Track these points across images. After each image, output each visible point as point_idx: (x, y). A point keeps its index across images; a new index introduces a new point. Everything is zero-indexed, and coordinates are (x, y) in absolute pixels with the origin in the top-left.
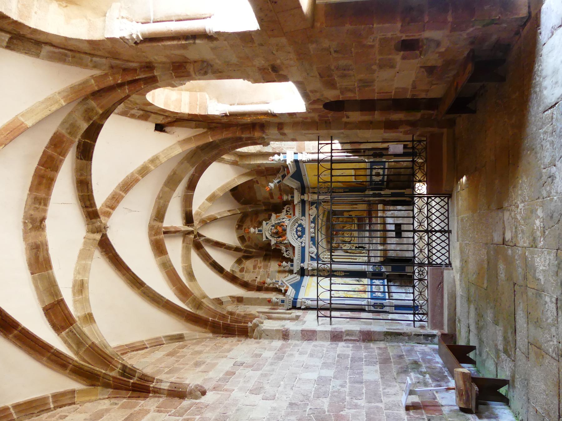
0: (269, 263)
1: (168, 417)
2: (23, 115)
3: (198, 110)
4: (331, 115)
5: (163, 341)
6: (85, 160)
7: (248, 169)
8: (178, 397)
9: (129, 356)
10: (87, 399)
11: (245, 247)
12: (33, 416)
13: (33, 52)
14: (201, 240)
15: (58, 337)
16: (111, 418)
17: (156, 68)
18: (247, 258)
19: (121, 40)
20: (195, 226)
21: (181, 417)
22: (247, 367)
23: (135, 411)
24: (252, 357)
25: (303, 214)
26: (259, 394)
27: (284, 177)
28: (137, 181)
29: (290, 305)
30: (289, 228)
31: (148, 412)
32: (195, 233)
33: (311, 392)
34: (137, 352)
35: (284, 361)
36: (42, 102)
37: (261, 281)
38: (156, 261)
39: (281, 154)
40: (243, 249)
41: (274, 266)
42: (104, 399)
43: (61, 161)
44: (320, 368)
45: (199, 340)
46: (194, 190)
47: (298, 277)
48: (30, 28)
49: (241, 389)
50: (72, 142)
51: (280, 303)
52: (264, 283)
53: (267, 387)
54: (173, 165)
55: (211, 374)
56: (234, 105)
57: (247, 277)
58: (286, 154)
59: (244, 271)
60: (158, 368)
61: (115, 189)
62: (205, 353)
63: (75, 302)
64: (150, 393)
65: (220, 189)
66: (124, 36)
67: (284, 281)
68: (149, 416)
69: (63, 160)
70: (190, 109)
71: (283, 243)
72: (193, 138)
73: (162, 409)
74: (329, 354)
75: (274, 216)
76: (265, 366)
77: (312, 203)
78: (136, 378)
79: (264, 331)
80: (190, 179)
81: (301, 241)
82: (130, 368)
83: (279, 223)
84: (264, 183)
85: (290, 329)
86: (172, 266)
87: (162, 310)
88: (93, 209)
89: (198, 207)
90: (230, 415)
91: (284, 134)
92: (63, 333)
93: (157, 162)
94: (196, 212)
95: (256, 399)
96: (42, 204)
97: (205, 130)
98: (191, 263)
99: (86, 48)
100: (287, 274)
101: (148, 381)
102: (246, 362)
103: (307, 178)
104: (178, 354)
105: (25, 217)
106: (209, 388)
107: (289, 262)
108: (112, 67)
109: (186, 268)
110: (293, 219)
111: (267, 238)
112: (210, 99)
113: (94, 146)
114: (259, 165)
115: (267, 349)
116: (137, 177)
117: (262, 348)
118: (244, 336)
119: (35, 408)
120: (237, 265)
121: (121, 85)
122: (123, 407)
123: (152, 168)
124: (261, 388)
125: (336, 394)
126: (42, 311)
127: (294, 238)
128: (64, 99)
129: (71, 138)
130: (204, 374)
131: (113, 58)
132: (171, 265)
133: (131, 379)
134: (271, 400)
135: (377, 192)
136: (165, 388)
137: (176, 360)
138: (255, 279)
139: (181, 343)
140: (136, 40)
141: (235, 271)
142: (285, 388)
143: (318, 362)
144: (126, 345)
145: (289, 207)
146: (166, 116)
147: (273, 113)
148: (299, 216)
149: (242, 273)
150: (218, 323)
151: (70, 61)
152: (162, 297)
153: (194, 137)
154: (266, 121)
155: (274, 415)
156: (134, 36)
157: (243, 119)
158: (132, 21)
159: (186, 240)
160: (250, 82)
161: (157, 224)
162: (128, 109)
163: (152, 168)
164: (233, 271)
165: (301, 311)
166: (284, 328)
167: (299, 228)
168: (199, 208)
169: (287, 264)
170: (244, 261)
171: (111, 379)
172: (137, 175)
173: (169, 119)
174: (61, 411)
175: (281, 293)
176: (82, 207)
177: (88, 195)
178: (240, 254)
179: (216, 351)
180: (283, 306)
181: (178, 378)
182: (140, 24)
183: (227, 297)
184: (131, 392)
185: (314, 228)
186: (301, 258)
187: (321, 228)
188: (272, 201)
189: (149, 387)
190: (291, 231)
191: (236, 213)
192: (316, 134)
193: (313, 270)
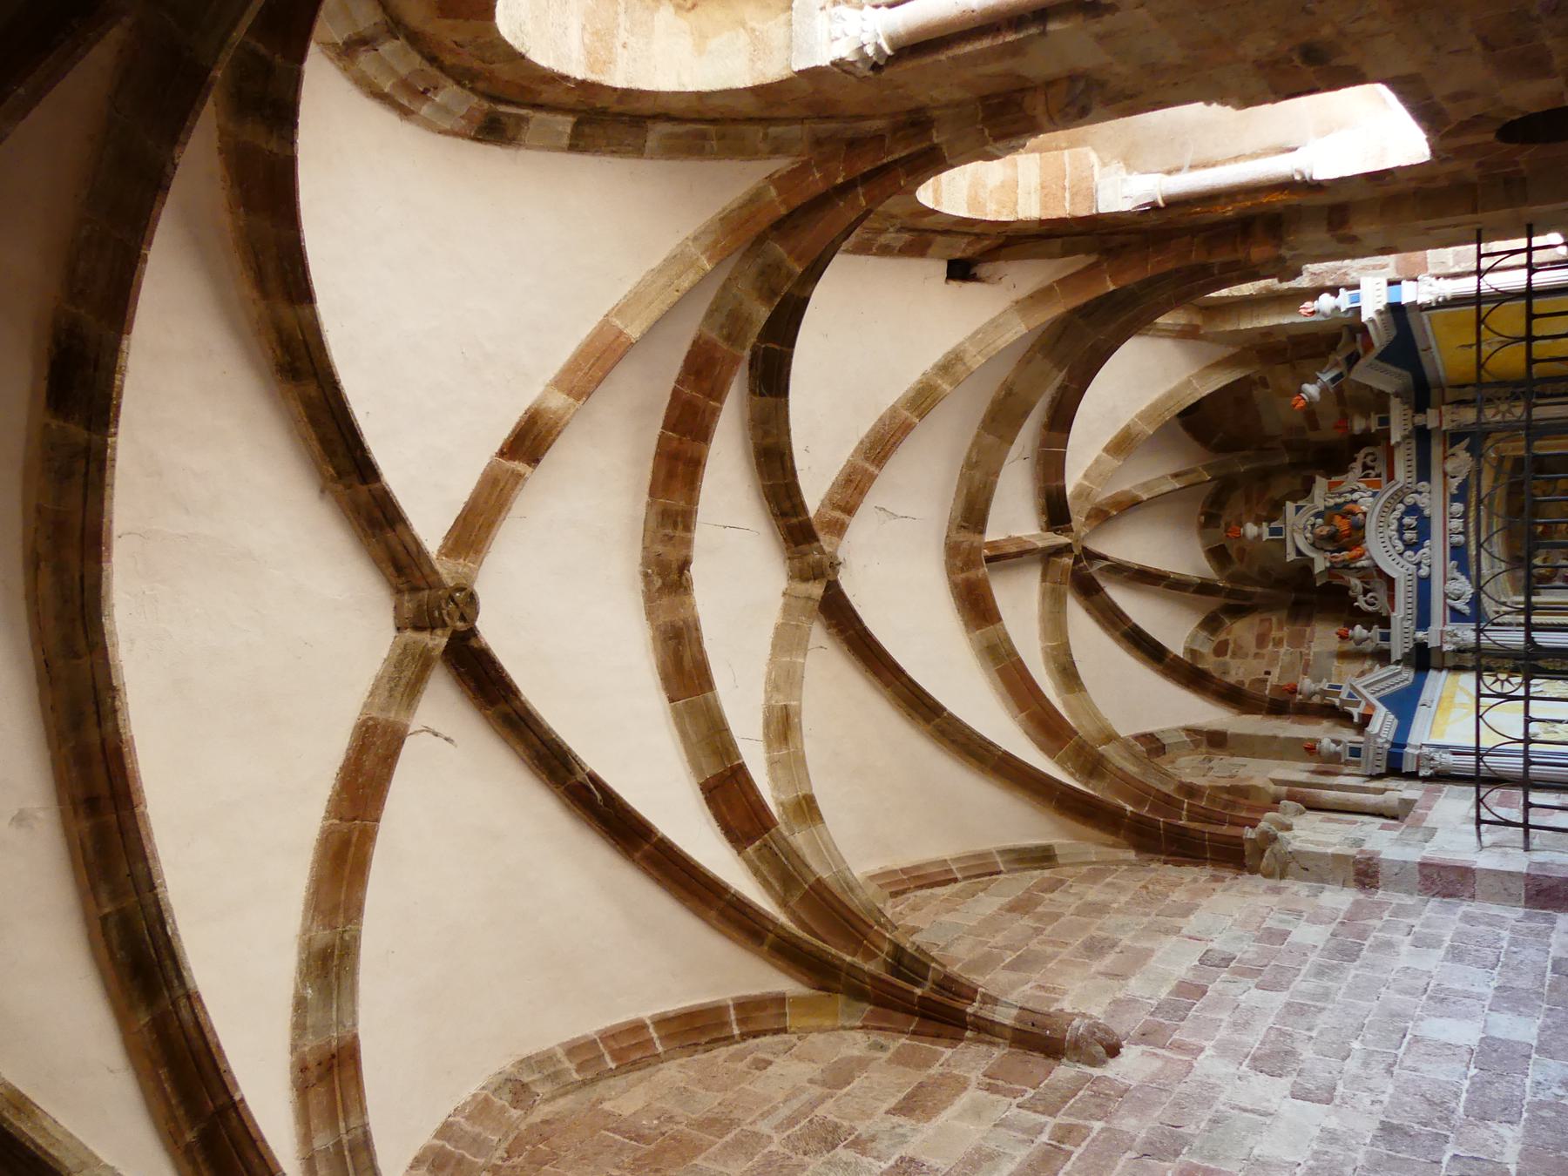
0: (1308, 630)
1: (1015, 1110)
2: (619, 310)
3: (1067, 205)
4: (1525, 157)
5: (996, 862)
6: (771, 395)
8: (1041, 1052)
9: (910, 901)
10: (812, 1022)
12: (696, 1051)
13: (629, 145)
15: (739, 859)
16: (871, 1089)
17: (936, 124)
18: (1238, 610)
19: (836, 69)
21: (1050, 1115)
22: (1243, 974)
23: (929, 1077)
24: (1258, 940)
25: (1424, 473)
26: (1280, 1076)
27: (1353, 360)
28: (906, 429)
30: (1374, 520)
31: (962, 1084)
33: (1457, 1096)
34: (930, 891)
35: (1361, 966)
36: (660, 271)
38: (971, 639)
40: (1223, 587)
41: (1324, 637)
42: (852, 1028)
43: (715, 413)
44: (1487, 1003)
45: (1096, 866)
46: (1069, 433)
47: (1405, 675)
48: (615, 89)
49: (1224, 1049)
50: (736, 361)
51: (1346, 756)
52: (1293, 691)
53: (1307, 1053)
54: (1004, 371)
55: (1135, 986)
56: (1178, 170)
57: (1238, 672)
58: (1357, 287)
59: (1229, 652)
60: (986, 949)
61: (852, 456)
62: (1118, 911)
63: (772, 763)
64: (967, 1029)
65: (1144, 416)
66: (843, 56)
67: (1359, 687)
68: (964, 1099)
69: (720, 409)
70: (1044, 206)
71: (1355, 568)
72: (1057, 288)
73: (1000, 1083)
74: (1520, 957)
75: (1321, 484)
76: (1299, 978)
77: (1455, 437)
78: (929, 984)
79: (1295, 855)
80: (1053, 399)
81: (1416, 558)
82: (913, 957)
85: (1382, 856)
86: (1016, 654)
87: (992, 779)
88: (800, 519)
90: (1192, 1135)
91: (1353, 239)
92: (748, 849)
93: (960, 368)
94: (1075, 488)
95: (1272, 1091)
96: (680, 526)
97: (1092, 259)
98: (1067, 638)
99: (748, 107)
100: (1367, 664)
101: (959, 995)
102: (1239, 955)
104: (1040, 909)
105: (646, 562)
106: (1128, 1033)
108: (818, 142)
110: (1388, 491)
111: (1299, 552)
112: (1104, 165)
113: (791, 356)
114: (1269, 332)
115: (1305, 915)
116: (906, 419)
117: (1290, 911)
118: (1231, 865)
119: (701, 1030)
120: (1205, 634)
121: (847, 188)
122: (900, 1059)
123: (946, 387)
124: (1286, 1053)
125: (1546, 1113)
126: (700, 793)
128: (708, 253)
129: (731, 349)
130: (1114, 983)
131: (820, 118)
132: (1012, 652)
133: (917, 984)
134: (1319, 1101)
136: (1007, 1022)
137: (1036, 929)
138: (1262, 676)
139: (1047, 873)
140: (875, 59)
141: (1201, 653)
142: (1366, 1064)
143: (1483, 983)
144: (903, 871)
145: (1372, 454)
146: (977, 235)
147: (1311, 178)
148: (1410, 480)
149: (1221, 658)
150: (1152, 823)
151: (716, 148)
152: (991, 743)
153: (1061, 282)
154: (1288, 207)
155: (1331, 1161)
156: (870, 51)
157: (1209, 211)
158: (861, 7)
160: (1228, 108)
161: (967, 538)
162: (870, 235)
163: (946, 387)
165: (1418, 784)
166: (1362, 852)
167: (1407, 520)
168: (1086, 476)
171: (868, 980)
172: (907, 413)
173: (986, 242)
174: (758, 1045)
176: (774, 515)
177: (786, 485)
178: (1214, 603)
179: (1147, 910)
180: (1358, 764)
181: (1041, 987)
182: (884, 9)
183: (1176, 730)
184: (917, 1019)
185: (1465, 516)
186: (1415, 603)
187: (1488, 539)
189: (964, 1012)
192: (1470, 224)
193: (1460, 651)
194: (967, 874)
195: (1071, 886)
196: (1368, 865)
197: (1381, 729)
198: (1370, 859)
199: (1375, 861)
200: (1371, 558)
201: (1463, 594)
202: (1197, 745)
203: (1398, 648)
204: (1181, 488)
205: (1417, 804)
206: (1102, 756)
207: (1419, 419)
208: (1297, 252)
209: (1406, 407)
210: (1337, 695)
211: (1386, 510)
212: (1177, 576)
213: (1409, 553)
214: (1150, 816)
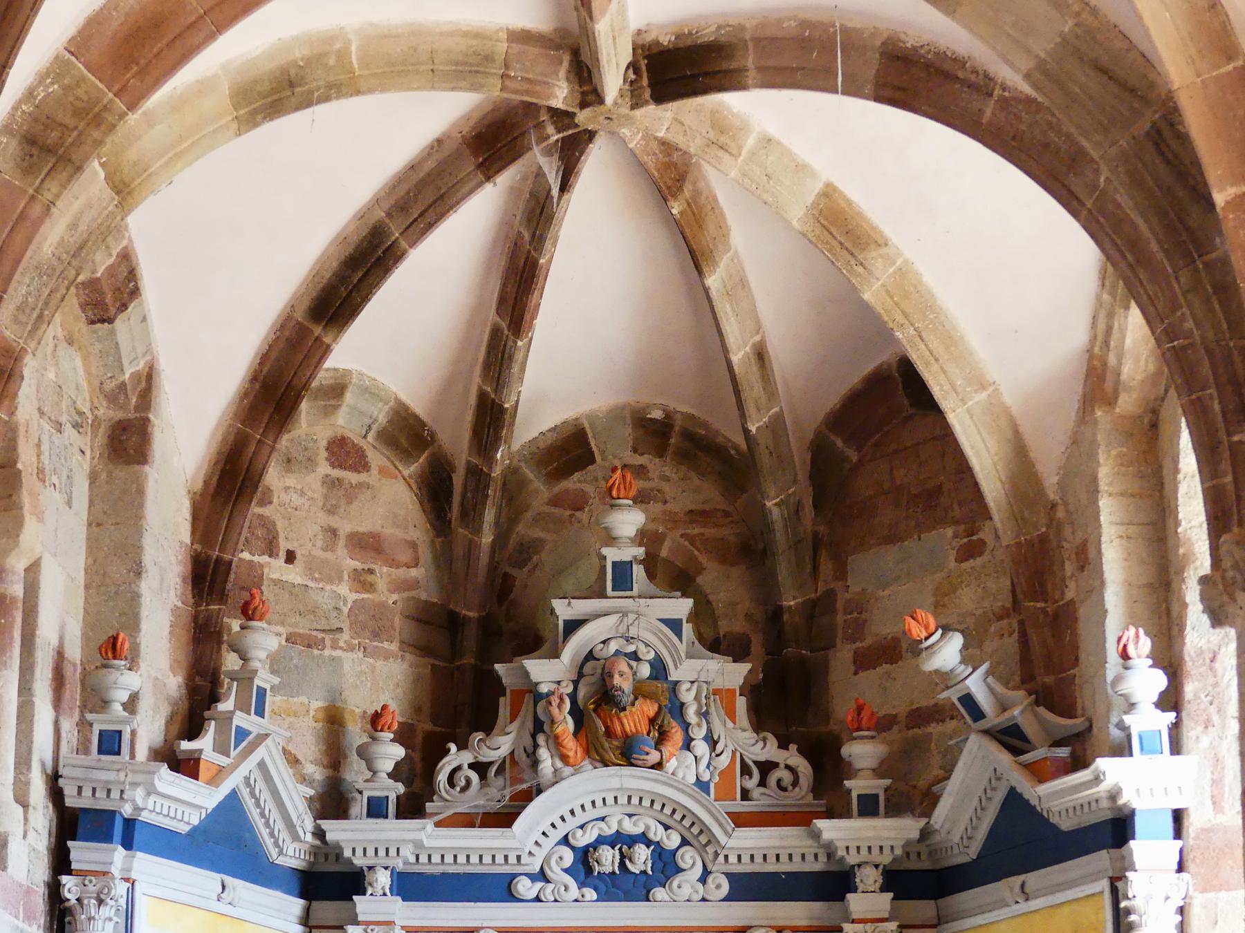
0: (394, 647)
7: (1062, 486)
11: (512, 472)
14: (543, 161)
20: (638, 113)
29: (87, 792)
32: (583, 118)
37: (268, 592)
39: (1171, 716)
46: (879, 99)
47: (291, 848)
51: (100, 723)
52: (248, 612)
58: (1176, 747)
59: (337, 473)
71: (536, 746)
75: (733, 674)
80: (960, 62)
81: (555, 872)
83: (679, 709)
84: (968, 599)
89: (772, 130)
98: (370, 91)
100: (316, 772)
103: (1004, 913)
107: (401, 788)
109: (332, 62)
111: (573, 626)
114: (1087, 558)
120: (382, 419)
127: (572, 823)
138: (283, 546)
141: (336, 407)
145: (795, 783)
148: (733, 859)
159: (534, 51)
164: (337, 390)
165: (42, 873)
168: (768, 141)
169: (390, 775)
170: (414, 468)
175: (175, 729)
180: (83, 748)
183: (149, 349)
188: (842, 656)
190: (623, 800)
191: (751, 409)
200: (557, 778)
202: (116, 396)
207: (869, 878)
209: (898, 852)
210: (243, 706)
212: (519, 356)
213: (569, 857)
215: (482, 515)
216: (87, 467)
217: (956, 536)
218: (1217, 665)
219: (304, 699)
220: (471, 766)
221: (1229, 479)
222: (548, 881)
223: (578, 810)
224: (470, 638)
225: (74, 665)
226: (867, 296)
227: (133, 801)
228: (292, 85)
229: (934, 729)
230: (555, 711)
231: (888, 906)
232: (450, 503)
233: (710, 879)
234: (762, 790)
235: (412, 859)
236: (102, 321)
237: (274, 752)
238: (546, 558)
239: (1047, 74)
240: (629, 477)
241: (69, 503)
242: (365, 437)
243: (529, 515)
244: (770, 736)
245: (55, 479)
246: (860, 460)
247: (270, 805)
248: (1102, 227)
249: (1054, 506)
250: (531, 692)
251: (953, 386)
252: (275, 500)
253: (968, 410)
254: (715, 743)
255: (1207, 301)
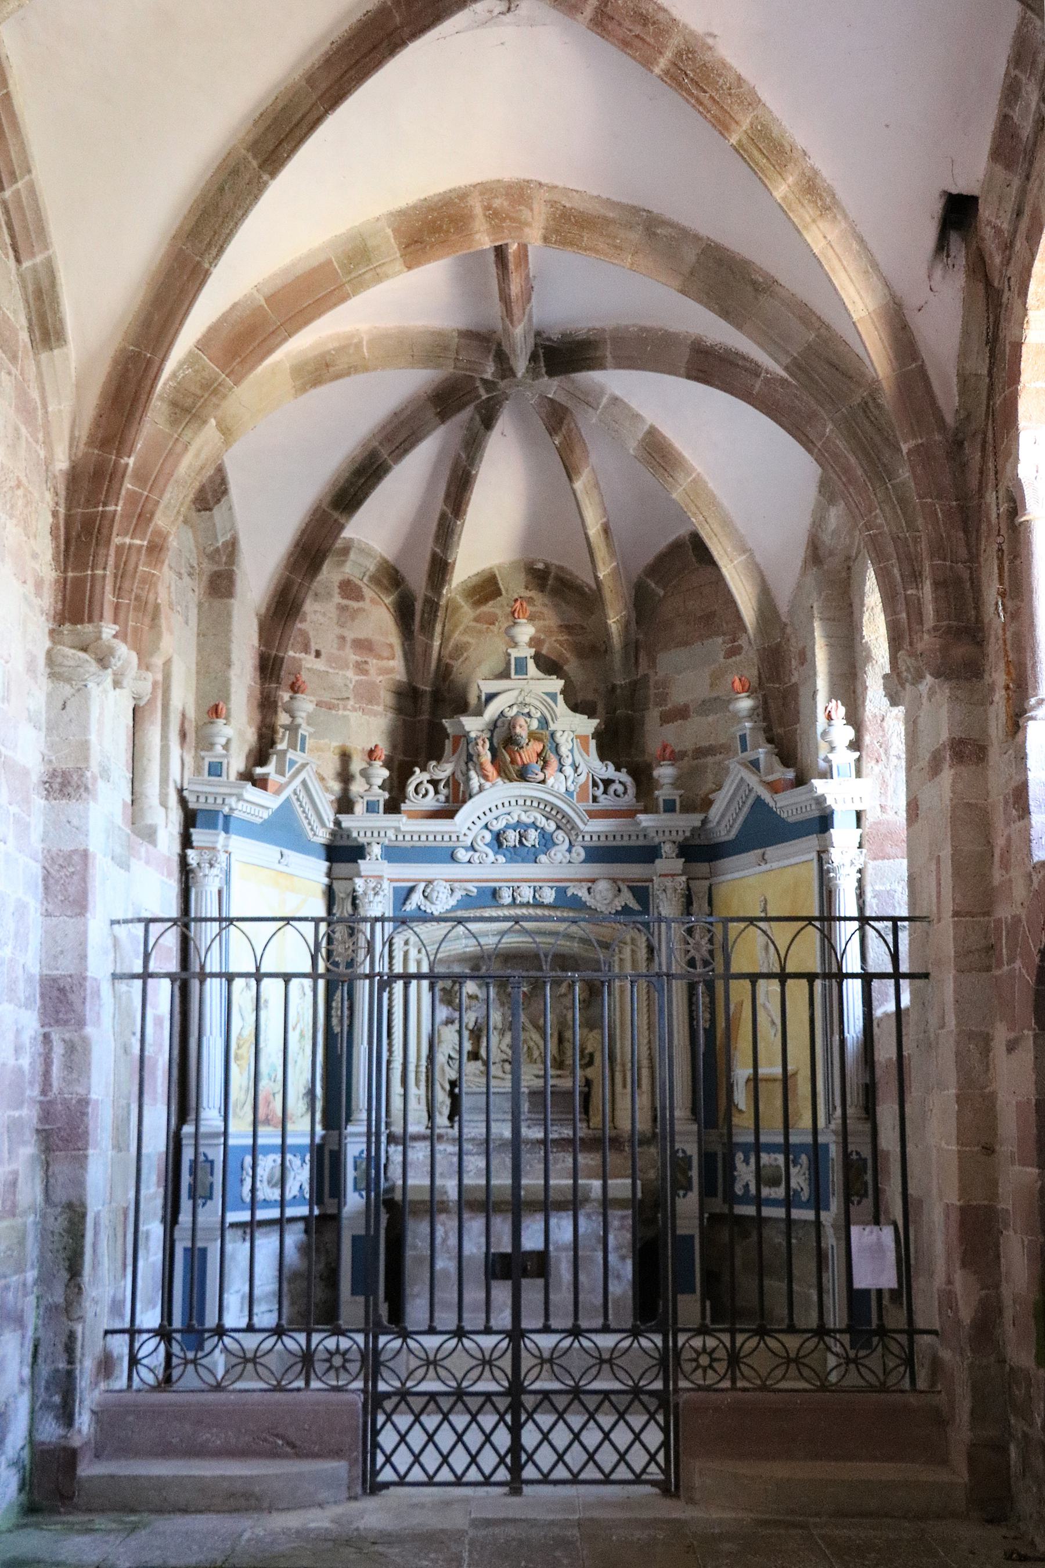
0: (380, 708)
5: (33, 255)
7: (791, 613)
37: (304, 676)
46: (689, 377)
52: (295, 688)
58: (859, 774)
59: (345, 602)
67: (303, 775)
71: (468, 770)
75: (587, 725)
80: (744, 358)
81: (480, 846)
85: (92, 804)
89: (618, 393)
91: (935, 768)
103: (751, 871)
107: (387, 795)
111: (491, 697)
114: (806, 658)
118: (60, 606)
120: (372, 568)
127: (490, 816)
132: (359, 285)
135: (694, 1173)
138: (314, 647)
139: (24, 336)
141: (344, 561)
145: (625, 793)
148: (587, 838)
149: (337, 590)
152: (221, 250)
164: (346, 551)
165: (176, 848)
166: (95, 779)
167: (533, 835)
168: (615, 400)
169: (380, 787)
173: (998, 260)
175: (252, 762)
178: (417, 581)
180: (198, 770)
183: (233, 527)
194: (11, 207)
195: (9, 373)
196: (78, 787)
197: (248, 801)
198: (86, 789)
199: (84, 795)
200: (481, 789)
201: (432, 903)
202: (213, 556)
203: (357, 823)
204: (587, 538)
205: (150, 847)
206: (205, 422)
207: (667, 849)
208: (924, 700)
209: (688, 834)
210: (292, 746)
211: (548, 809)
212: (458, 530)
213: (488, 837)
214: (123, 492)
215: (434, 627)
216: (196, 599)
217: (724, 642)
218: (885, 724)
219: (327, 741)
220: (428, 782)
221: (904, 615)
222: (475, 851)
223: (494, 809)
224: (426, 704)
225: (191, 721)
226: (674, 496)
227: (230, 805)
228: (327, 365)
229: (710, 760)
230: (480, 748)
231: (681, 867)
232: (413, 620)
233: (574, 850)
234: (605, 796)
235: (394, 838)
236: (206, 509)
237: (311, 774)
238: (472, 653)
239: (799, 367)
240: (525, 605)
241: (187, 623)
242: (362, 580)
243: (461, 628)
244: (609, 763)
245: (179, 609)
246: (664, 596)
247: (308, 806)
248: (827, 460)
249: (786, 625)
250: (463, 736)
251: (725, 551)
252: (308, 619)
253: (734, 567)
254: (577, 768)
255: (894, 507)
